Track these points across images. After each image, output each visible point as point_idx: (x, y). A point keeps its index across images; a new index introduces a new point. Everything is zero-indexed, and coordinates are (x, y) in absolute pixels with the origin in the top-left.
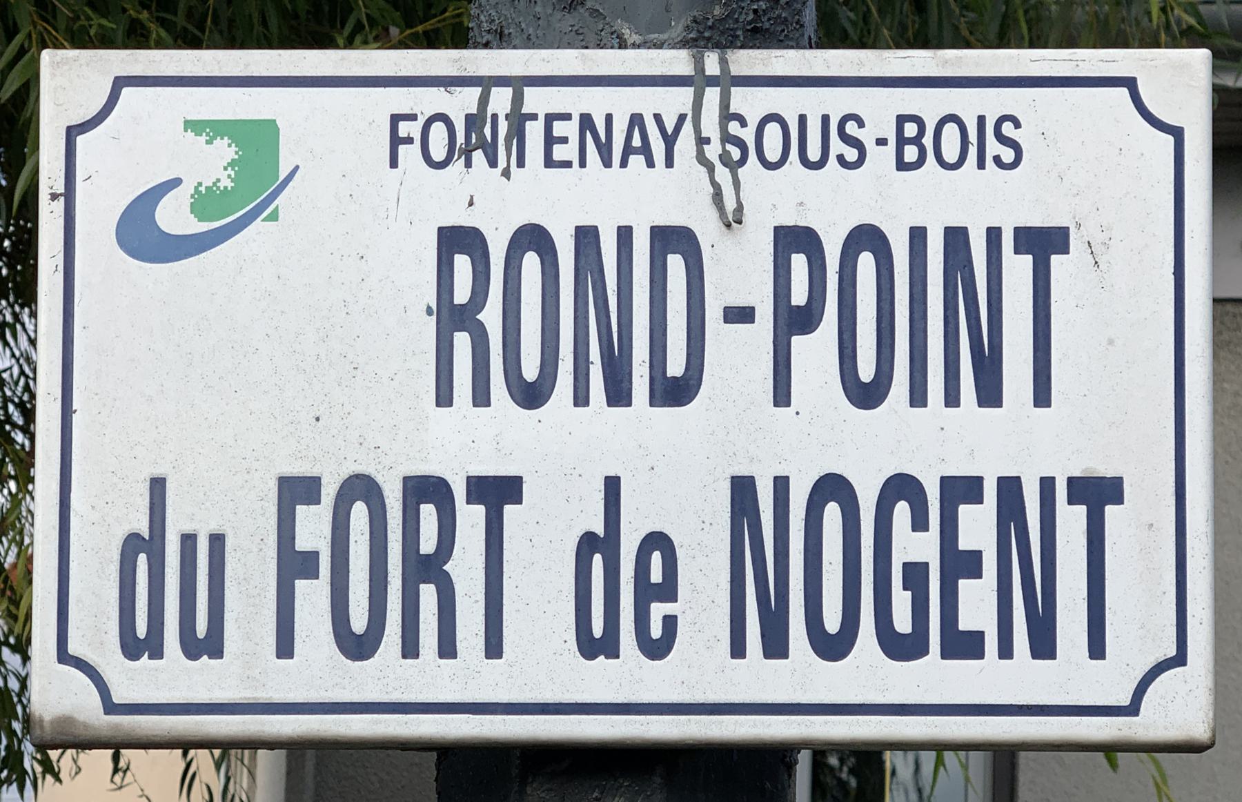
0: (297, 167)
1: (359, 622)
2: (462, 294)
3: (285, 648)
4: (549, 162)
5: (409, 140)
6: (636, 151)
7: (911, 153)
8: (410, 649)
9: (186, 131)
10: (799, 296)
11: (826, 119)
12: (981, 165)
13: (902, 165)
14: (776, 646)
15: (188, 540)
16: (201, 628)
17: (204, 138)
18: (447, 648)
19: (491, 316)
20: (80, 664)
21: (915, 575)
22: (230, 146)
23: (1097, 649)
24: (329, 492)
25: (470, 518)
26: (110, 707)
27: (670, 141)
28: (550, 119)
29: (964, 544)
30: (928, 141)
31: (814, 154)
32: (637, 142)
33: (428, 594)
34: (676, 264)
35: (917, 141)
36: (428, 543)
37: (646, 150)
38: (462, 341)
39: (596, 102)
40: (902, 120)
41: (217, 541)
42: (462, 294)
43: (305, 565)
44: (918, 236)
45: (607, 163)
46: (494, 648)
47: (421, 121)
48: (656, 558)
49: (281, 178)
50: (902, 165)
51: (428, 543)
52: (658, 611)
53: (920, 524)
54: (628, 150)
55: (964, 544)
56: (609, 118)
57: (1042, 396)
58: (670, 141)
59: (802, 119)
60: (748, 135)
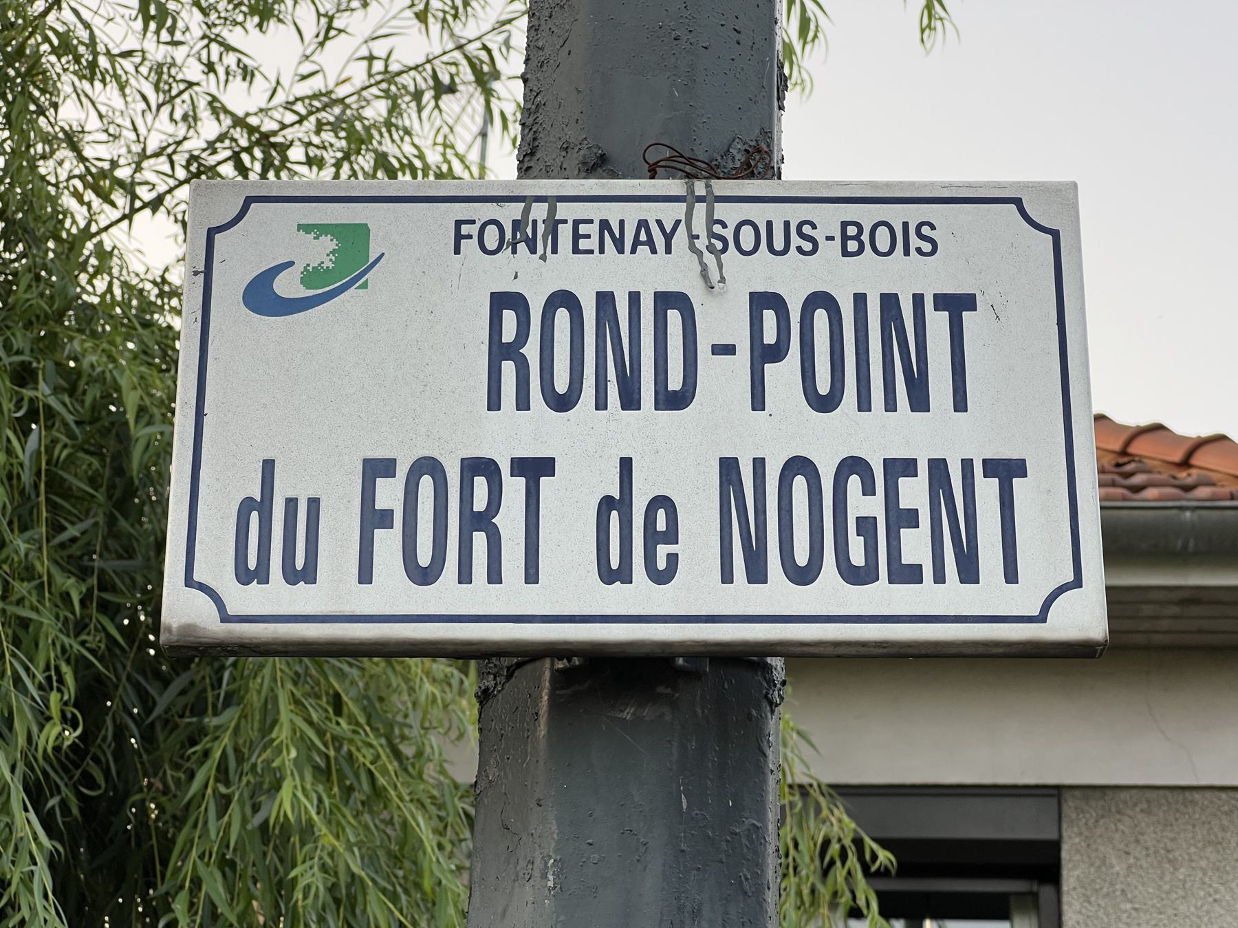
0: (383, 254)
1: (424, 557)
2: (508, 335)
3: (365, 575)
4: (576, 250)
5: (470, 237)
6: (643, 243)
7: (852, 246)
8: (465, 576)
9: (298, 230)
10: (770, 337)
11: (787, 224)
12: (907, 253)
13: (845, 253)
14: (757, 574)
15: (291, 503)
16: (300, 563)
17: (313, 235)
18: (494, 576)
19: (531, 351)
20: (203, 587)
21: (866, 526)
22: (332, 240)
23: (1011, 575)
24: (402, 470)
25: (514, 488)
26: (225, 618)
27: (668, 237)
28: (577, 223)
29: (903, 505)
30: (865, 237)
31: (779, 245)
32: (643, 237)
33: (480, 539)
34: (674, 317)
35: (857, 238)
36: (480, 504)
37: (650, 242)
38: (508, 369)
39: (612, 213)
40: (845, 225)
41: (314, 503)
42: (508, 335)
43: (385, 520)
44: (860, 300)
45: (621, 250)
46: (532, 576)
47: (478, 225)
48: (661, 514)
49: (371, 261)
50: (845, 253)
51: (480, 504)
52: (662, 551)
53: (869, 490)
54: (636, 243)
55: (903, 505)
56: (622, 223)
57: (960, 404)
58: (668, 237)
59: (769, 224)
60: (729, 234)
